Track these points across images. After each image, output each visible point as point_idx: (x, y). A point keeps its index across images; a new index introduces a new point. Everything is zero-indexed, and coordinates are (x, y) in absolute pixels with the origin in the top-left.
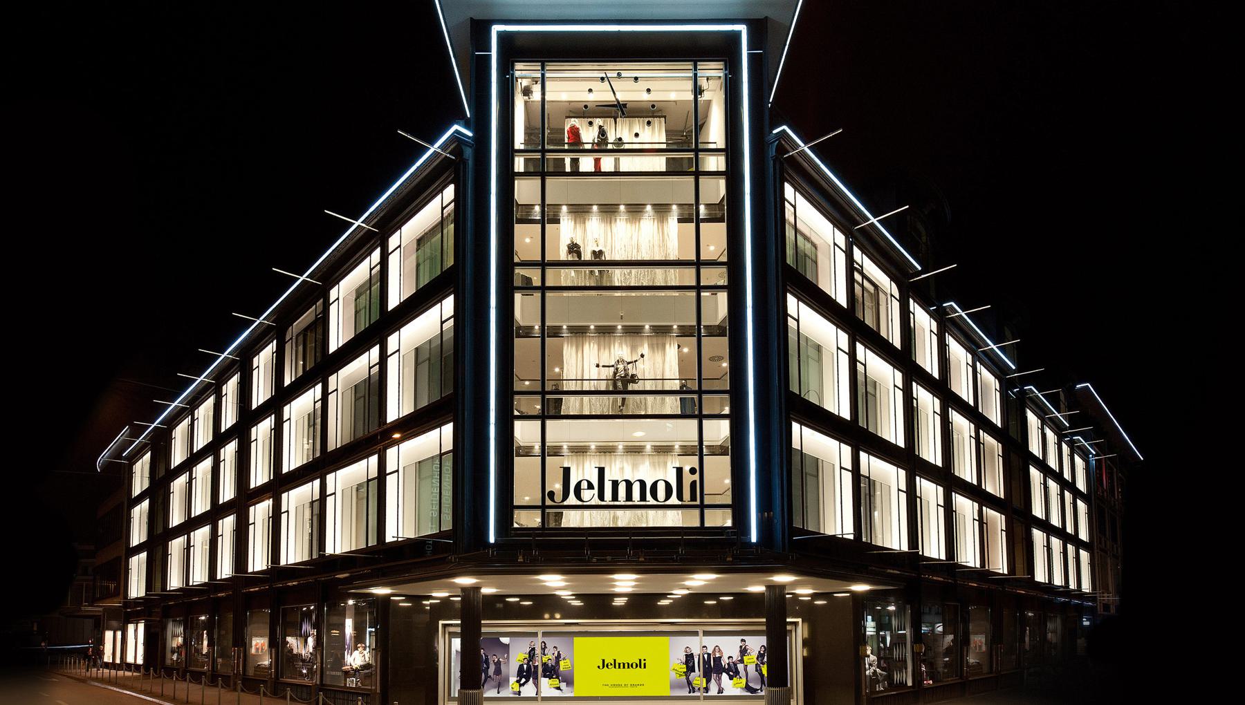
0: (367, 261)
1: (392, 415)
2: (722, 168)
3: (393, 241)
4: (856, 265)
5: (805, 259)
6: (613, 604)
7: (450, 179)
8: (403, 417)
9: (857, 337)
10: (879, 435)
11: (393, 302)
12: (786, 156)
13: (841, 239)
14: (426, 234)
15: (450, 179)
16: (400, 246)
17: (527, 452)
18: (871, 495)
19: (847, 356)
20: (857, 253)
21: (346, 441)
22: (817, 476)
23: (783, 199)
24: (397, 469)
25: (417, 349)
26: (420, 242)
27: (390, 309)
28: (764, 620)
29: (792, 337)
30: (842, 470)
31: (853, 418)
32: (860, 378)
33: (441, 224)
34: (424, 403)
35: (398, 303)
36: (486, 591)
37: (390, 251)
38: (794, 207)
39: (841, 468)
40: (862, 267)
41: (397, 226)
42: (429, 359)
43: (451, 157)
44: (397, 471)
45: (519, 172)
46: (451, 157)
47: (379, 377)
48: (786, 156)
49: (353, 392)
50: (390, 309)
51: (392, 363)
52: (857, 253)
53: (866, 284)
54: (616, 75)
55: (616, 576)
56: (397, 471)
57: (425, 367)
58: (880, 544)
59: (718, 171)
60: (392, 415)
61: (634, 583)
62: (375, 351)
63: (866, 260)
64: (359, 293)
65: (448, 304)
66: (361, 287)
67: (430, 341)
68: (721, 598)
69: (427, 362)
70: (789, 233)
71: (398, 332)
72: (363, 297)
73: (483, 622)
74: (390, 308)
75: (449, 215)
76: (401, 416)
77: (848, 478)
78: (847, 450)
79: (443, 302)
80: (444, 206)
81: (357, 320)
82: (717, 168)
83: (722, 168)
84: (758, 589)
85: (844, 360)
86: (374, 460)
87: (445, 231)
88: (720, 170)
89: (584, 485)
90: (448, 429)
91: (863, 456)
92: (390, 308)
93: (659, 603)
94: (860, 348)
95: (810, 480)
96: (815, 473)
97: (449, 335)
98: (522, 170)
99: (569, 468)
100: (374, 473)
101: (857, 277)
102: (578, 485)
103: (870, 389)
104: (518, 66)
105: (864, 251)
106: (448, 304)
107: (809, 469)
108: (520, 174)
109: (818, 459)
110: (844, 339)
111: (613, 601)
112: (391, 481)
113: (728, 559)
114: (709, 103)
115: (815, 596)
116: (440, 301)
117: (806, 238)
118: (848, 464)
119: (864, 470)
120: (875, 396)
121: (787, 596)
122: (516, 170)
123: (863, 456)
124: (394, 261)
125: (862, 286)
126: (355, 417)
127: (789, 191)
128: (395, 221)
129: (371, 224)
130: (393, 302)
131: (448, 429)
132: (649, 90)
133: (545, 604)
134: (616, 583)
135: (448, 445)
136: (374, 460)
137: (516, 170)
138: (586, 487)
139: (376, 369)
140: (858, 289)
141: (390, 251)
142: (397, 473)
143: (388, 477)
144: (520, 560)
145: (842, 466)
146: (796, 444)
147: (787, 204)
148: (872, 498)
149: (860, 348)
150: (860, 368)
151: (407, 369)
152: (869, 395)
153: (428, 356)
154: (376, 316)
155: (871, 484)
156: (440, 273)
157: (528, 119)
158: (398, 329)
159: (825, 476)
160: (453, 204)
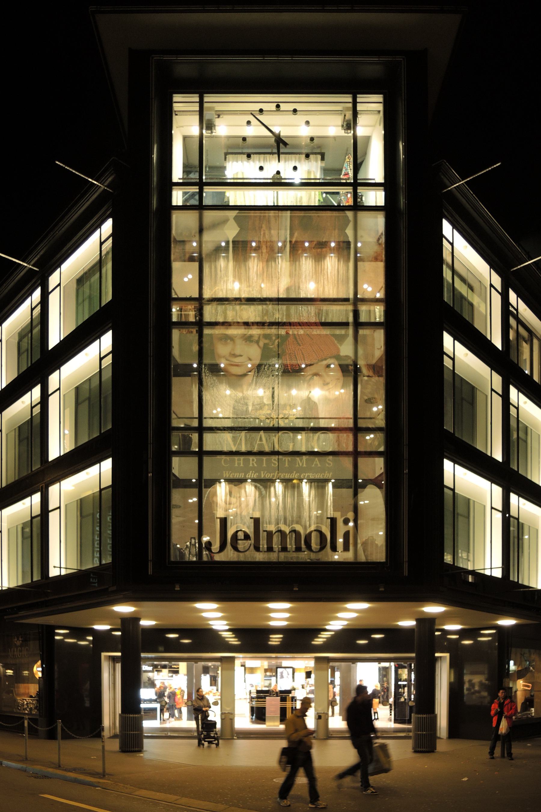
0: (28, 301)
1: (54, 454)
2: (381, 202)
3: (54, 280)
4: (511, 309)
5: (461, 301)
6: (270, 643)
7: (109, 212)
8: (64, 455)
9: (511, 380)
10: (529, 478)
11: (53, 341)
12: (445, 190)
13: (497, 280)
14: (85, 273)
15: (109, 212)
16: (59, 285)
17: (185, 484)
18: (519, 538)
19: (500, 399)
20: (513, 296)
21: (11, 480)
22: (468, 517)
23: (441, 236)
24: (59, 506)
25: (77, 389)
26: (81, 281)
27: (50, 348)
28: (413, 655)
29: (447, 377)
30: (493, 510)
31: (505, 460)
32: (513, 423)
33: (100, 264)
34: (84, 439)
35: (59, 341)
36: (145, 623)
37: (50, 393)
38: (452, 244)
39: (492, 508)
40: (517, 310)
41: (56, 265)
42: (89, 399)
43: (108, 189)
44: (59, 508)
45: (177, 206)
46: (108, 189)
47: (41, 422)
48: (445, 190)
49: (17, 434)
50: (50, 348)
51: (53, 402)
52: (513, 296)
53: (521, 330)
54: (273, 107)
55: (272, 605)
56: (59, 508)
57: (85, 407)
58: (526, 583)
59: (376, 206)
60: (54, 454)
61: (287, 615)
62: (37, 391)
63: (521, 303)
64: (22, 335)
65: (107, 340)
66: (23, 330)
67: (90, 380)
68: (373, 636)
69: (87, 402)
70: (447, 274)
71: (58, 371)
72: (25, 340)
73: (143, 655)
74: (51, 347)
75: (108, 253)
76: (62, 454)
77: (498, 517)
78: (498, 491)
79: (102, 338)
80: (102, 241)
81: (20, 365)
82: (376, 202)
83: (381, 202)
84: (409, 623)
85: (497, 401)
86: (37, 498)
87: (104, 271)
88: (378, 205)
89: (241, 535)
90: (107, 465)
91: (514, 498)
92: (51, 347)
93: (313, 643)
94: (513, 391)
95: (461, 521)
96: (466, 515)
97: (108, 375)
98: (180, 203)
99: (211, 685)
100: (37, 510)
101: (513, 322)
102: (235, 535)
103: (521, 435)
104: (177, 98)
105: (519, 295)
106: (107, 340)
107: (460, 509)
108: (178, 208)
109: (469, 499)
110: (497, 380)
111: (268, 639)
112: (53, 518)
113: (381, 589)
114: (368, 139)
115: (463, 634)
116: (99, 337)
117: (463, 280)
118: (498, 505)
119: (513, 512)
120: (526, 442)
121: (437, 633)
122: (174, 203)
123: (514, 498)
124: (54, 299)
125: (517, 332)
126: (19, 468)
127: (447, 228)
128: (55, 259)
129: (32, 263)
130: (53, 341)
131: (107, 465)
132: (307, 123)
133: (231, 338)
134: (272, 615)
135: (107, 481)
136: (37, 498)
137: (174, 203)
138: (243, 538)
139: (39, 308)
140: (512, 335)
141: (50, 393)
142: (58, 510)
143: (50, 514)
144: (177, 588)
145: (493, 506)
146: (448, 480)
147: (445, 242)
148: (520, 541)
149: (513, 391)
150: (513, 411)
151: (68, 409)
152: (520, 440)
153: (87, 395)
154: (37, 356)
155: (520, 526)
156: (98, 309)
157: (186, 153)
158: (59, 368)
159: (476, 515)
160: (111, 239)
